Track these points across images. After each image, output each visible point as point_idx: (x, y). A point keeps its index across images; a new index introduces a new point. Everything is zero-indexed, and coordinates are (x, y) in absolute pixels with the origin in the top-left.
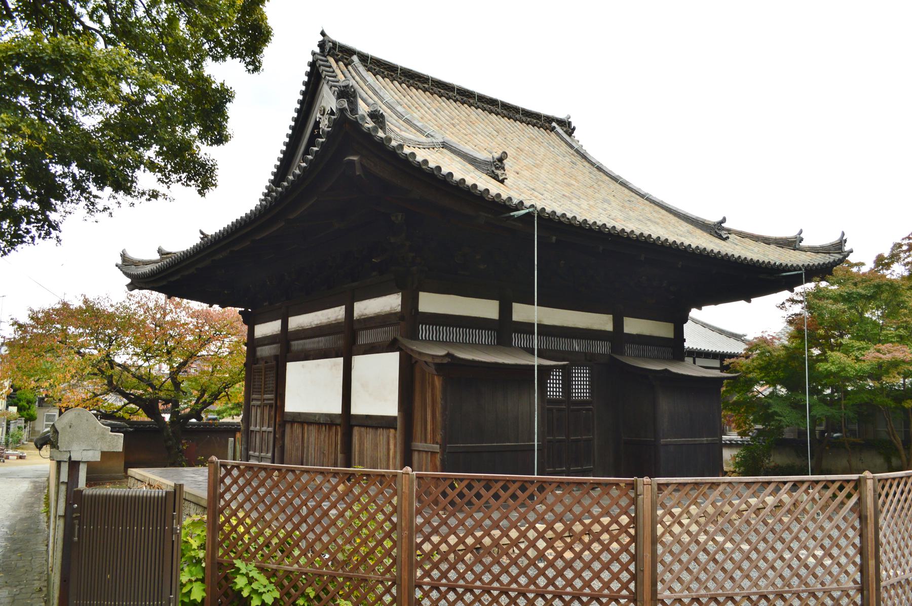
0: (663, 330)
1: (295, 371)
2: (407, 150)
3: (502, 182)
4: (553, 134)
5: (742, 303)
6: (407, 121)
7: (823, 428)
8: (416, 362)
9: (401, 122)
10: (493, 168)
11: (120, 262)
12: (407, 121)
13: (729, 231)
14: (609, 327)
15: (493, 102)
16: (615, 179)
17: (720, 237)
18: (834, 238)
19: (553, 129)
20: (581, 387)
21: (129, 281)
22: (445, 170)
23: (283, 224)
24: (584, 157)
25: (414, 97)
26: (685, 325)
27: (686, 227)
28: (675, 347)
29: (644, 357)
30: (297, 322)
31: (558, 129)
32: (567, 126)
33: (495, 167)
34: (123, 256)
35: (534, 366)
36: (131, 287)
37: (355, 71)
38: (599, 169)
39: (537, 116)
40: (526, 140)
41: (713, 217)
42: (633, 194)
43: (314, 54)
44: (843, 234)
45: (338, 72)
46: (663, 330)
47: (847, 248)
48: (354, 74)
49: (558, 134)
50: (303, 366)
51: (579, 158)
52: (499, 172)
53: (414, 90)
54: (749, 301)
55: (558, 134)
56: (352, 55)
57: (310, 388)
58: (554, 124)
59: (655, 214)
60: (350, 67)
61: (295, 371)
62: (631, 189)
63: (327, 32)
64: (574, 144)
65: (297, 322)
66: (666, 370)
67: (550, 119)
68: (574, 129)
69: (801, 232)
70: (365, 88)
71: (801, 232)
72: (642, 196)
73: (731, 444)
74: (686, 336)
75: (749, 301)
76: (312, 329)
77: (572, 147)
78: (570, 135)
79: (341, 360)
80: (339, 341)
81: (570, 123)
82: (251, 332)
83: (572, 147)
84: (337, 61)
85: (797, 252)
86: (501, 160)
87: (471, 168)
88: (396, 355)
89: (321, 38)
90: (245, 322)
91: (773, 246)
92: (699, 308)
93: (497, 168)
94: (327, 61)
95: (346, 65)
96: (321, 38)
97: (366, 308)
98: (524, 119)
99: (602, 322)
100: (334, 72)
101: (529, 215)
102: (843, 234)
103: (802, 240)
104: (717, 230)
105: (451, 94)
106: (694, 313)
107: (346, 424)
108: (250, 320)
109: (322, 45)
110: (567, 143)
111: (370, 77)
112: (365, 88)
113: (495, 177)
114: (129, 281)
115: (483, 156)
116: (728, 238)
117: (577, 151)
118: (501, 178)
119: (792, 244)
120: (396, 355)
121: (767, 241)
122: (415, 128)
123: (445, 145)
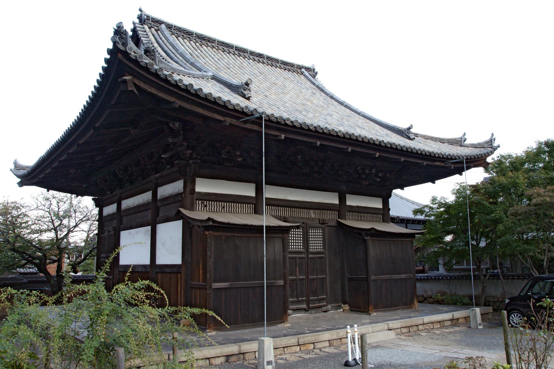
0: (377, 204)
1: (125, 236)
2: (176, 77)
3: (248, 99)
4: (302, 77)
5: (430, 184)
6: (192, 64)
7: (488, 266)
8: (193, 226)
9: (188, 64)
10: (242, 90)
11: (13, 167)
12: (192, 64)
13: (416, 135)
14: (337, 202)
15: (260, 56)
16: (341, 103)
17: (409, 138)
18: (487, 138)
19: (302, 73)
20: (316, 243)
21: (19, 180)
22: (196, 87)
23: (92, 132)
24: (322, 90)
25: (204, 51)
26: (390, 200)
27: (361, 121)
28: (384, 214)
29: (361, 220)
30: (127, 203)
31: (306, 73)
32: (312, 72)
33: (241, 90)
34: (15, 163)
35: (263, 226)
36: (21, 184)
37: (162, 34)
38: (332, 97)
39: (292, 65)
40: (282, 79)
41: (403, 126)
42: (353, 113)
43: (134, 23)
44: (493, 135)
45: (150, 34)
46: (377, 204)
47: (495, 144)
48: (161, 36)
49: (305, 76)
50: (129, 233)
51: (319, 91)
52: (246, 92)
53: (205, 47)
54: (434, 183)
55: (305, 76)
56: (161, 24)
57: (133, 249)
58: (303, 70)
59: (365, 124)
60: (159, 32)
61: (125, 236)
62: (352, 110)
63: (143, 9)
64: (315, 82)
65: (127, 203)
66: (373, 229)
67: (300, 67)
68: (316, 73)
69: (465, 134)
70: (168, 44)
71: (465, 134)
72: (359, 114)
73: (424, 279)
74: (391, 206)
75: (434, 183)
76: (134, 208)
77: (314, 84)
78: (314, 77)
79: (149, 227)
80: (149, 215)
81: (314, 70)
82: (101, 213)
83: (314, 84)
84: (150, 28)
85: (462, 148)
86: (247, 84)
87: (229, 91)
88: (179, 223)
89: (140, 13)
90: (97, 206)
91: (446, 144)
92: (402, 188)
93: (244, 90)
94: (143, 28)
95: (156, 31)
96: (140, 13)
97: (165, 191)
98: (282, 66)
99: (332, 199)
100: (147, 35)
101: (260, 118)
102: (493, 135)
103: (465, 140)
104: (405, 133)
105: (231, 50)
106: (394, 191)
107: (152, 271)
108: (99, 204)
109: (140, 18)
110: (311, 81)
111: (173, 38)
112: (168, 44)
113: (244, 96)
114: (19, 180)
115: (235, 81)
116: (414, 138)
117: (318, 87)
118: (247, 96)
119: (459, 142)
120: (179, 223)
121: (442, 141)
122: (196, 68)
123: (214, 78)
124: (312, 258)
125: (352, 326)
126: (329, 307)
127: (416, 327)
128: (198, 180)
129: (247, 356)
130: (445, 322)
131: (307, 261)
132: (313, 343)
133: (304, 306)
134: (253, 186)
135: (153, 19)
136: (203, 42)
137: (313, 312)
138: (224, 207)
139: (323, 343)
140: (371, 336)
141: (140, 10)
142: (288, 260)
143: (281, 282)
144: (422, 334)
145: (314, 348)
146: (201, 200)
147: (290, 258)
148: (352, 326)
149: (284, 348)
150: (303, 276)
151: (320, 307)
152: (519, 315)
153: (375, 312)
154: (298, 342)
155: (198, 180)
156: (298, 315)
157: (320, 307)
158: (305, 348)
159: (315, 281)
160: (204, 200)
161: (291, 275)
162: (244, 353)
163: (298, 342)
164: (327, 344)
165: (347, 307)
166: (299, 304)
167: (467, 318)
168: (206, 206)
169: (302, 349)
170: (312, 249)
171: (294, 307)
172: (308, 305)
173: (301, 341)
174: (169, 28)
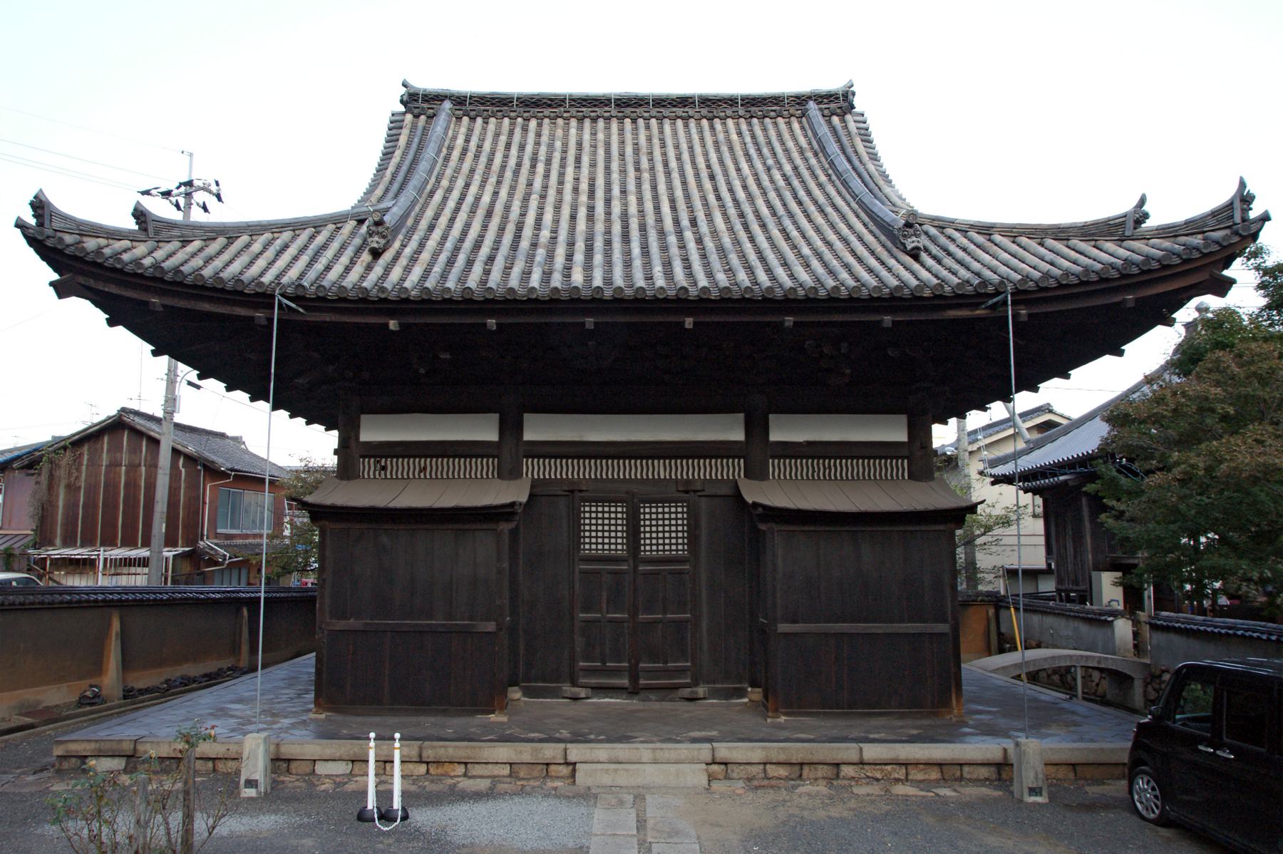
20: (665, 532)
89: (404, 90)
124: (646, 574)
125: (385, 738)
126: (701, 690)
127: (936, 769)
128: (528, 418)
129: (293, 765)
130: (966, 769)
131: (633, 575)
132: (466, 764)
133: (625, 682)
134: (903, 419)
135: (425, 95)
136: (753, 109)
137: (652, 697)
138: (425, 468)
139: (490, 766)
140: (627, 770)
141: (405, 85)
142: (577, 575)
143: (491, 626)
144: (855, 790)
145: (465, 775)
146: (374, 457)
147: (583, 572)
148: (385, 738)
149: (801, 764)
150: (622, 612)
151: (676, 688)
152: (1158, 792)
153: (786, 714)
154: (420, 756)
155: (528, 418)
156: (607, 700)
157: (676, 688)
158: (440, 771)
159: (660, 626)
160: (381, 457)
161: (586, 609)
162: (289, 760)
163: (420, 756)
164: (506, 770)
165: (756, 694)
166: (609, 676)
167: (1002, 769)
168: (384, 468)
169: (432, 771)
170: (648, 548)
171: (594, 681)
172: (634, 678)
173: (429, 754)
174: (460, 104)
